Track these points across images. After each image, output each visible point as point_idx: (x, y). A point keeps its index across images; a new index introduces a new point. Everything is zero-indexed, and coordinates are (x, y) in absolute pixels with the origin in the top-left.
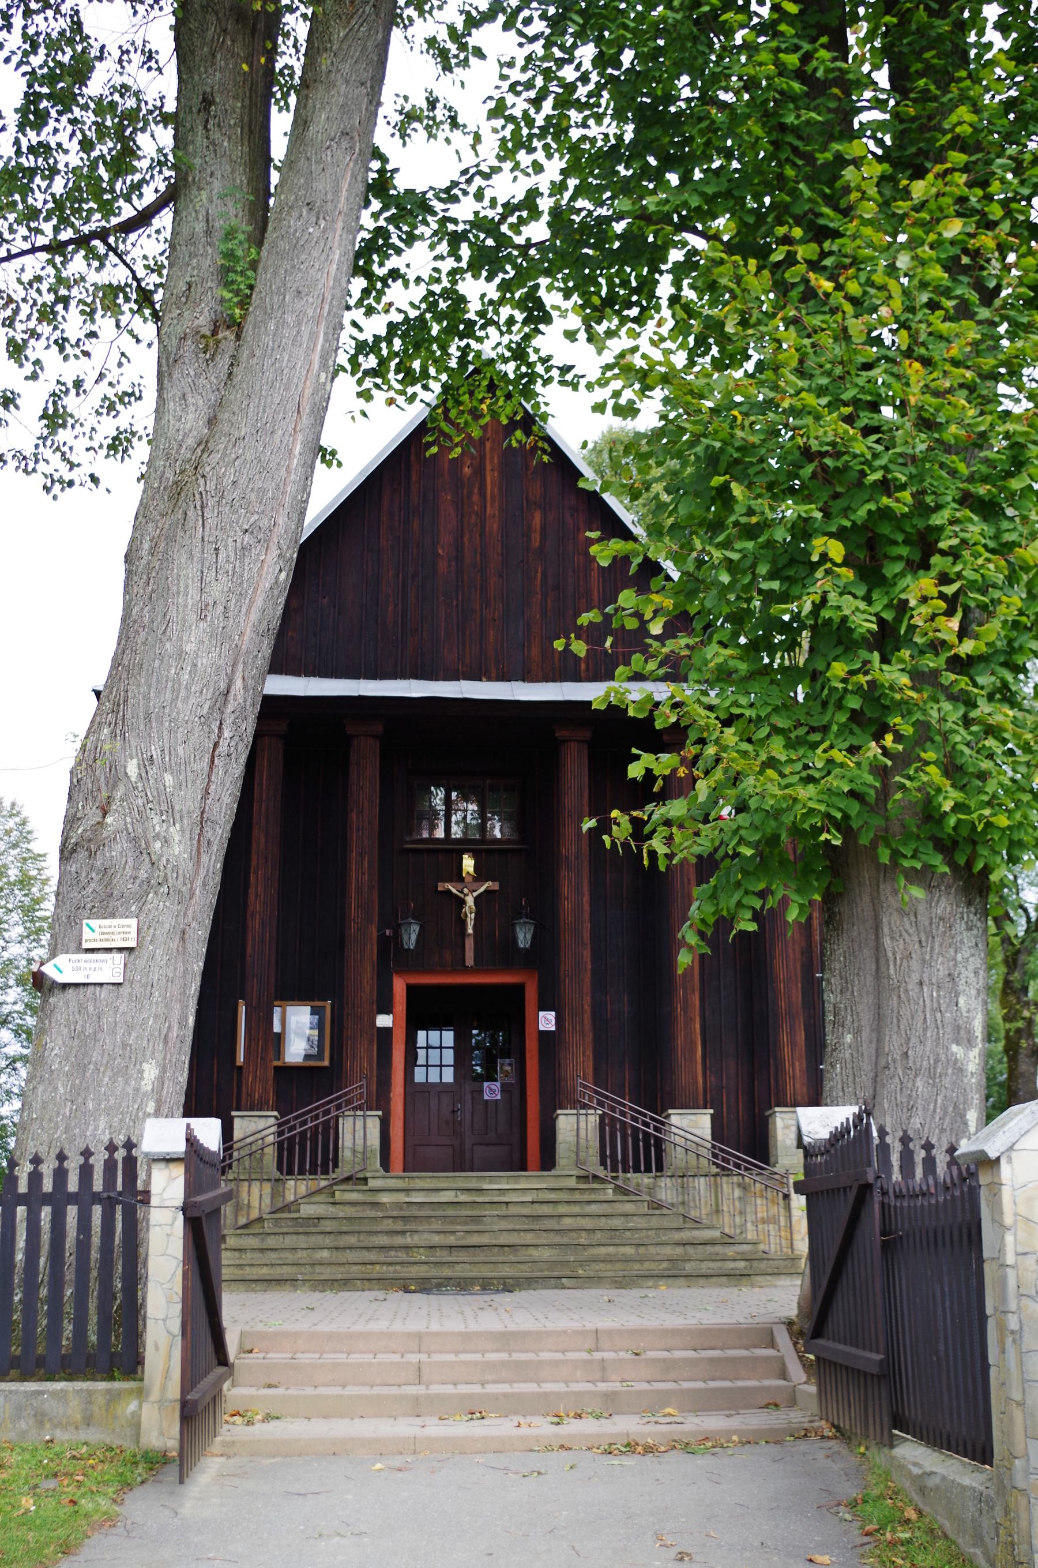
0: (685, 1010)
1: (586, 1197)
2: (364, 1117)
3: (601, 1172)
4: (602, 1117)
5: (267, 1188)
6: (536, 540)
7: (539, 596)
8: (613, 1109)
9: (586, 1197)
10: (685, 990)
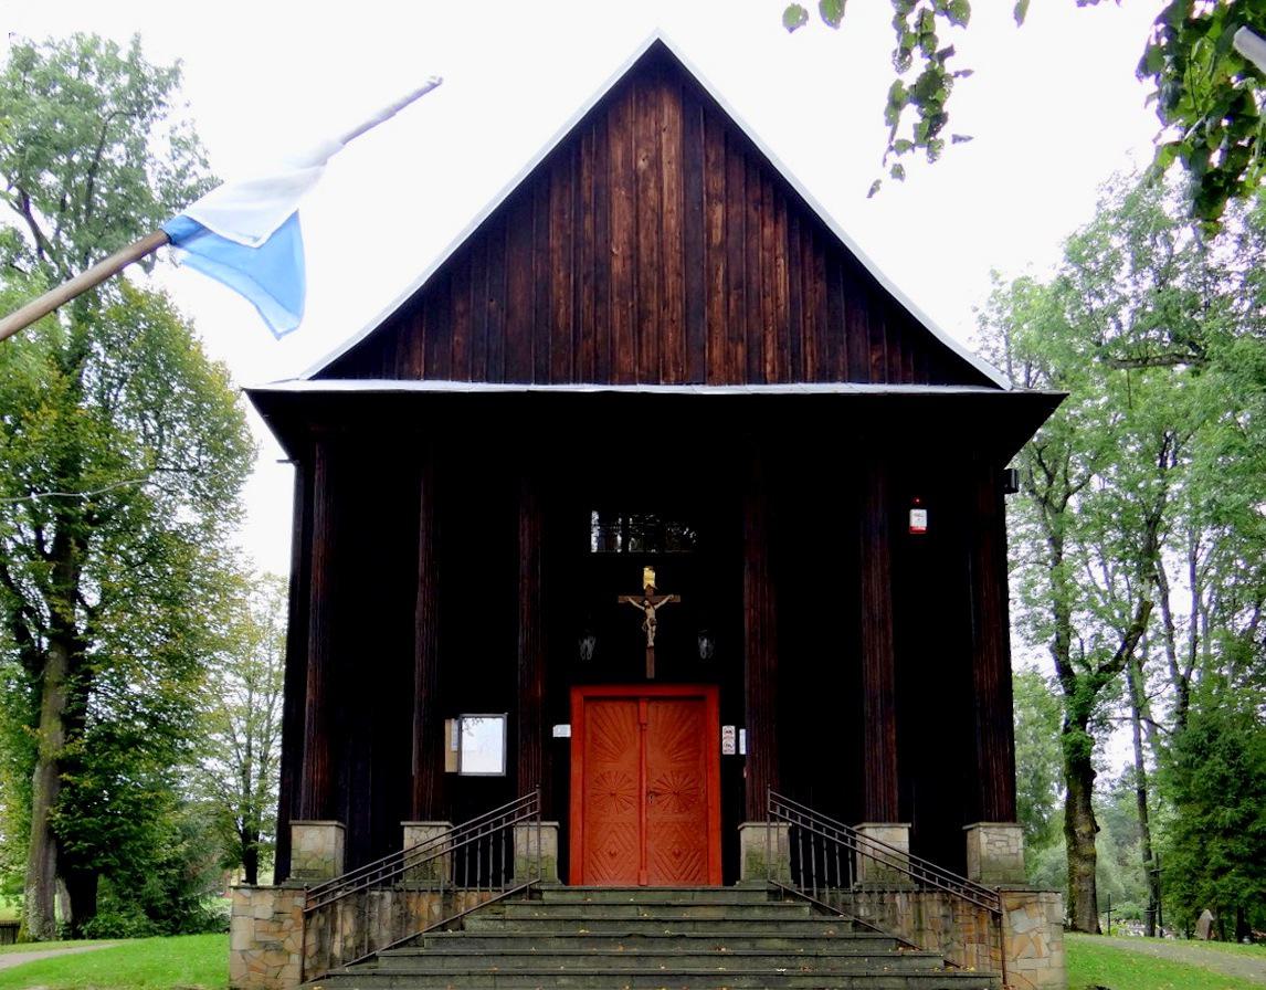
2: (539, 827)
4: (793, 832)
6: (717, 235)
7: (721, 295)
8: (805, 821)
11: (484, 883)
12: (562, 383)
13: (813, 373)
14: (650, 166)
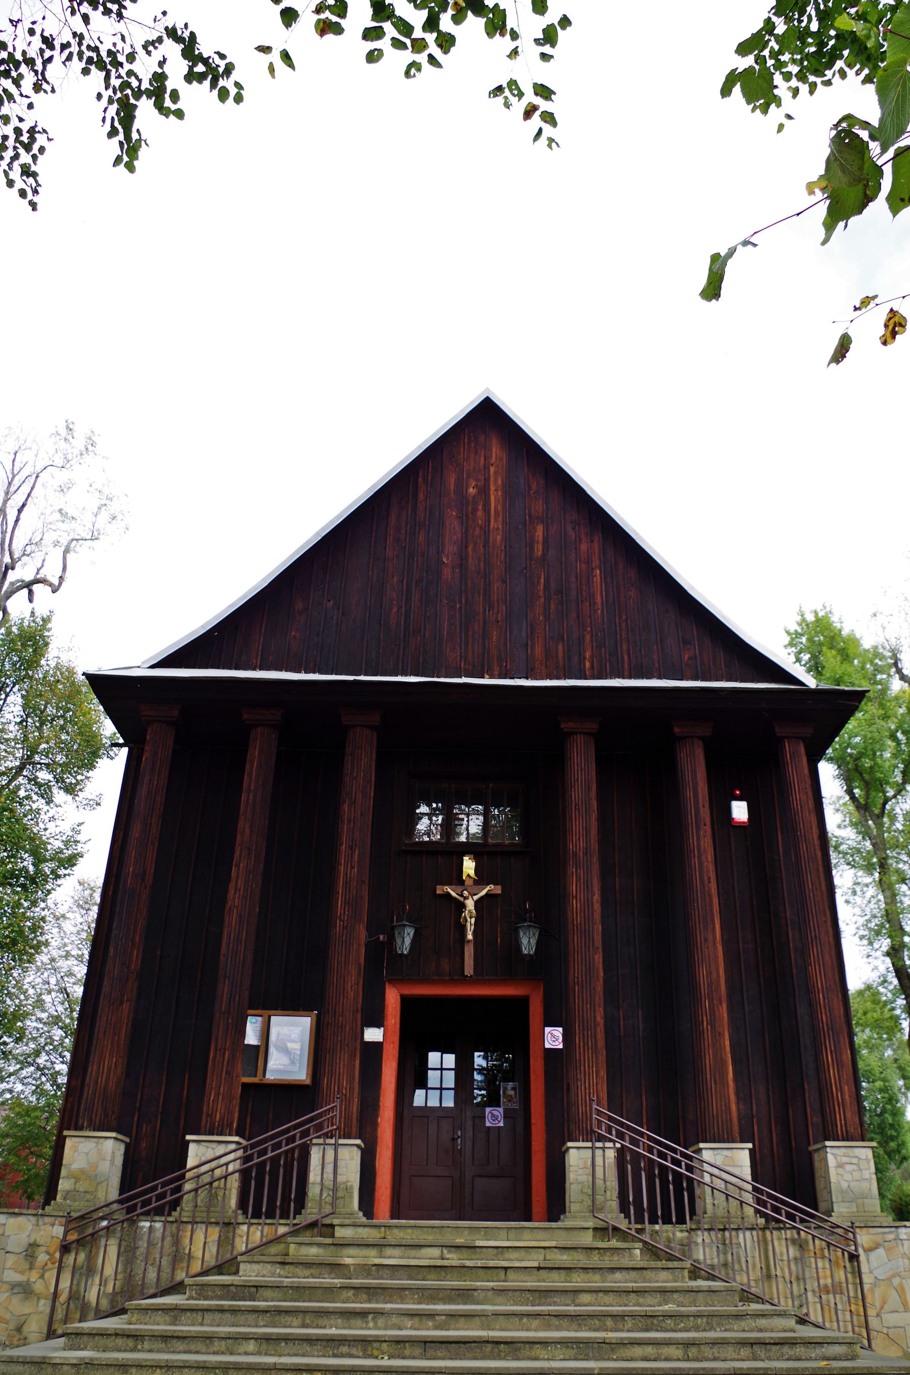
0: (712, 1023)
1: (608, 1261)
2: (336, 1146)
3: (623, 1224)
4: (621, 1153)
5: (214, 1233)
6: (539, 550)
7: (542, 600)
8: (634, 1142)
9: (608, 1261)
10: (711, 1000)
11: (270, 1215)
14: (479, 492)
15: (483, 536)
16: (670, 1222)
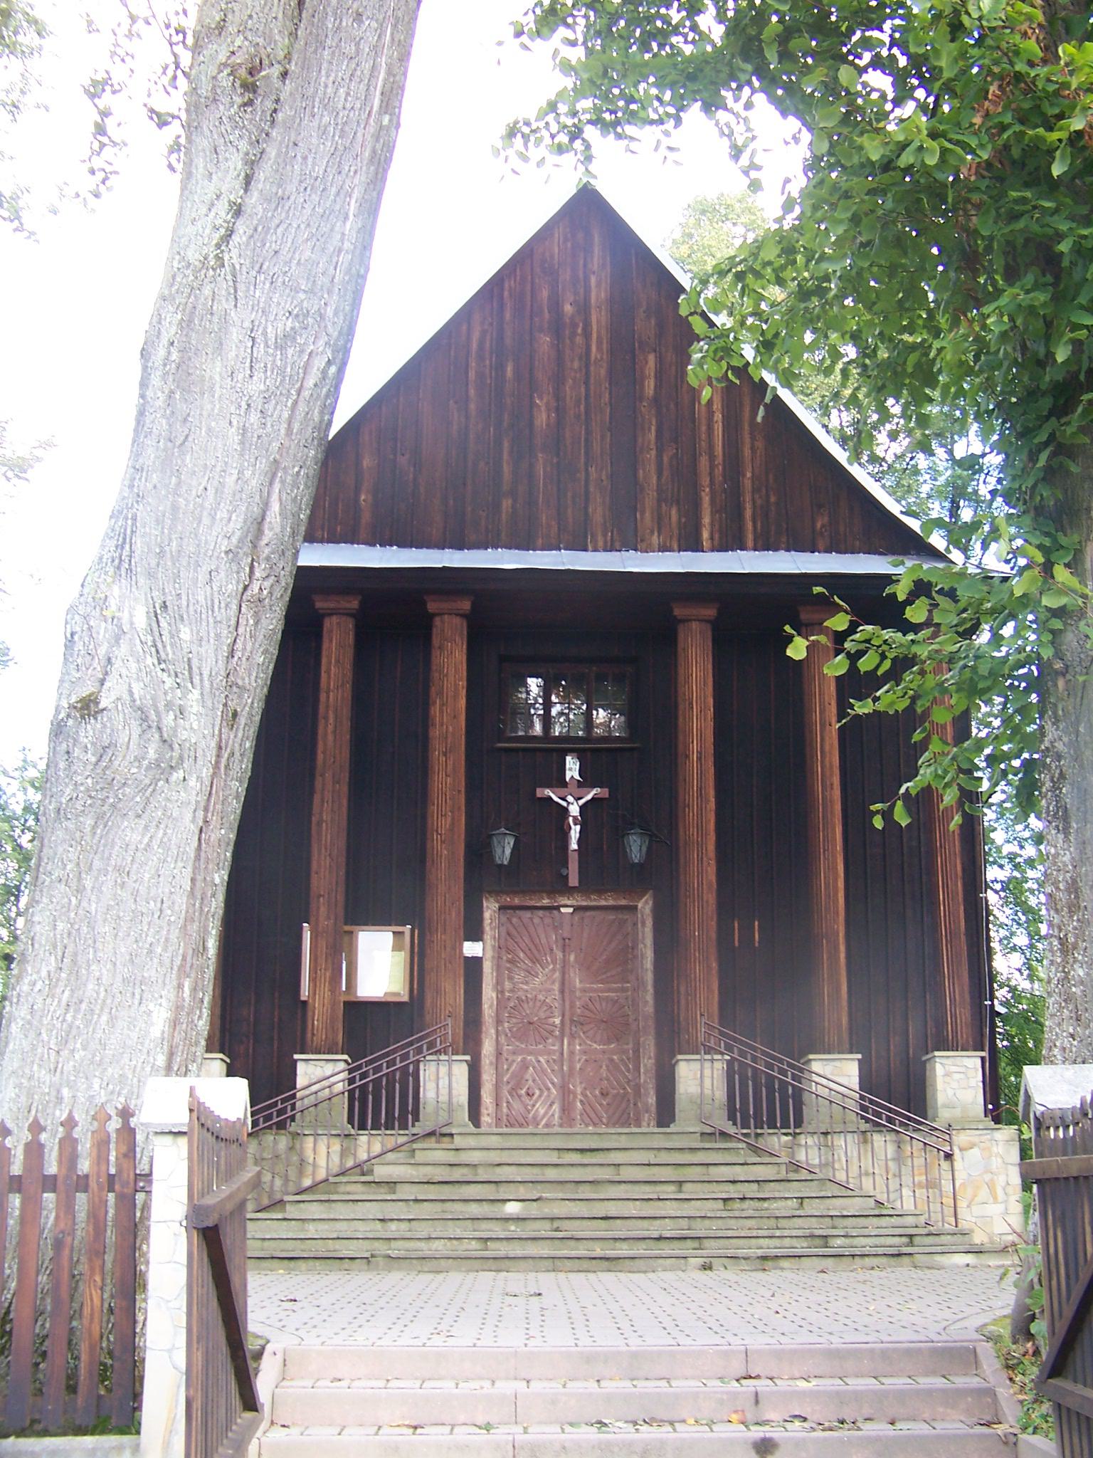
3: (731, 1130)
4: (730, 1063)
5: (336, 1146)
7: (653, 453)
11: (389, 1126)
12: (484, 545)
13: (755, 540)
15: (584, 371)
16: (775, 1127)
